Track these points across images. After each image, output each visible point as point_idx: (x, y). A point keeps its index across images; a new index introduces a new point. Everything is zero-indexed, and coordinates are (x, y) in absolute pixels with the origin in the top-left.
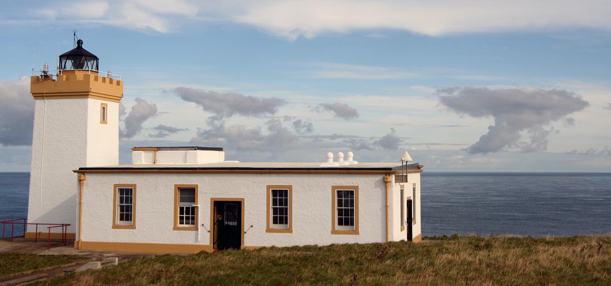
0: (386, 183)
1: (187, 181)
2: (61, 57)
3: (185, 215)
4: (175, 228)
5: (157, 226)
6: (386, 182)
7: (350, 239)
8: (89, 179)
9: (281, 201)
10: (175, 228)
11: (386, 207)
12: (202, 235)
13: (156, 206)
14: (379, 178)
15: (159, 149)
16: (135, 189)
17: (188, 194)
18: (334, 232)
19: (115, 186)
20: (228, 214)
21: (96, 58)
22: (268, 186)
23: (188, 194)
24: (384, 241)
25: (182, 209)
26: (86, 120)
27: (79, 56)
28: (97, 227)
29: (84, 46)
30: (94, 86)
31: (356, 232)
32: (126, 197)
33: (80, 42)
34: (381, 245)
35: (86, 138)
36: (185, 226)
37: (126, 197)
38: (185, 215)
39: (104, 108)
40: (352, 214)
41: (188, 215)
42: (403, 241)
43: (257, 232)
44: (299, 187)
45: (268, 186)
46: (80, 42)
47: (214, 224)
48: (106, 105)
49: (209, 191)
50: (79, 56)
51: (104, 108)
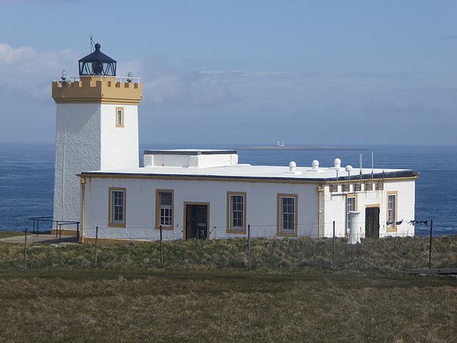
2: (80, 61)
3: (165, 217)
5: (140, 228)
6: (319, 192)
12: (176, 232)
13: (141, 208)
14: (313, 187)
16: (297, 199)
17: (165, 197)
18: (229, 231)
19: (110, 189)
21: (115, 62)
23: (165, 197)
25: (162, 210)
26: (100, 125)
27: (98, 61)
28: (97, 229)
29: (101, 50)
30: (106, 92)
32: (118, 199)
33: (98, 46)
35: (100, 142)
36: (237, 227)
38: (165, 217)
39: (120, 112)
40: (121, 211)
41: (165, 217)
42: (409, 237)
43: (218, 227)
44: (250, 191)
46: (98, 46)
47: (187, 224)
48: (123, 109)
50: (98, 61)
51: (120, 112)
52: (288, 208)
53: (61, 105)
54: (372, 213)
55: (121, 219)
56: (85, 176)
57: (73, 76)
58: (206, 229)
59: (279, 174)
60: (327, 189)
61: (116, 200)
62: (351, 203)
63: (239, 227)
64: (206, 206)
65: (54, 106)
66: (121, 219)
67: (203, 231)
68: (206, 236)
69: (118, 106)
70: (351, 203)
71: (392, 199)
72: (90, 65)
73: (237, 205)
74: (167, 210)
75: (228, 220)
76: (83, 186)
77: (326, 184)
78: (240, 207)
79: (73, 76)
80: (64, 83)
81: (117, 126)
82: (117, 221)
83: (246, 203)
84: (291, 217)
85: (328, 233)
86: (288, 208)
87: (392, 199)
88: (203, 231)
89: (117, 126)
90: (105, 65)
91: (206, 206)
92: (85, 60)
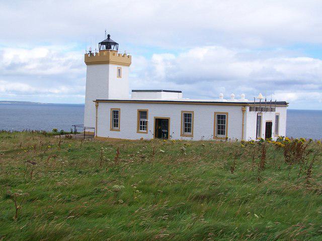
0: (244, 111)
1: (116, 106)
3: (142, 125)
4: (137, 132)
5: (129, 131)
7: (188, 139)
8: (100, 105)
9: (189, 119)
10: (137, 132)
11: (243, 125)
13: (129, 117)
14: (239, 108)
15: (160, 91)
16: (227, 116)
17: (143, 114)
18: (182, 135)
20: (162, 125)
21: (115, 44)
22: (215, 112)
23: (143, 114)
24: (240, 140)
27: (108, 44)
28: (104, 131)
31: (192, 136)
32: (116, 114)
33: (109, 36)
34: (318, 143)
36: (142, 131)
37: (116, 114)
39: (119, 70)
40: (117, 122)
41: (143, 125)
43: (175, 130)
44: (197, 111)
45: (215, 112)
46: (109, 36)
47: (156, 131)
48: (121, 68)
49: (154, 113)
50: (108, 44)
51: (119, 70)
52: (221, 120)
53: (90, 66)
54: (269, 125)
55: (117, 126)
56: (98, 101)
57: (95, 49)
58: (167, 133)
59: (214, 98)
60: (248, 108)
61: (115, 115)
62: (259, 119)
63: (222, 135)
64: (156, 119)
65: (85, 68)
66: (117, 126)
67: (165, 135)
68: (167, 137)
69: (118, 66)
70: (259, 119)
71: (277, 117)
72: (105, 46)
73: (187, 119)
74: (144, 122)
75: (181, 128)
76: (97, 106)
77: (247, 105)
78: (189, 120)
79: (95, 49)
80: (92, 54)
81: (117, 77)
82: (186, 133)
83: (193, 118)
84: (223, 127)
85: (247, 139)
86: (221, 120)
87: (277, 117)
88: (165, 135)
89: (117, 77)
90: (112, 46)
91: (156, 119)
92: (102, 43)
